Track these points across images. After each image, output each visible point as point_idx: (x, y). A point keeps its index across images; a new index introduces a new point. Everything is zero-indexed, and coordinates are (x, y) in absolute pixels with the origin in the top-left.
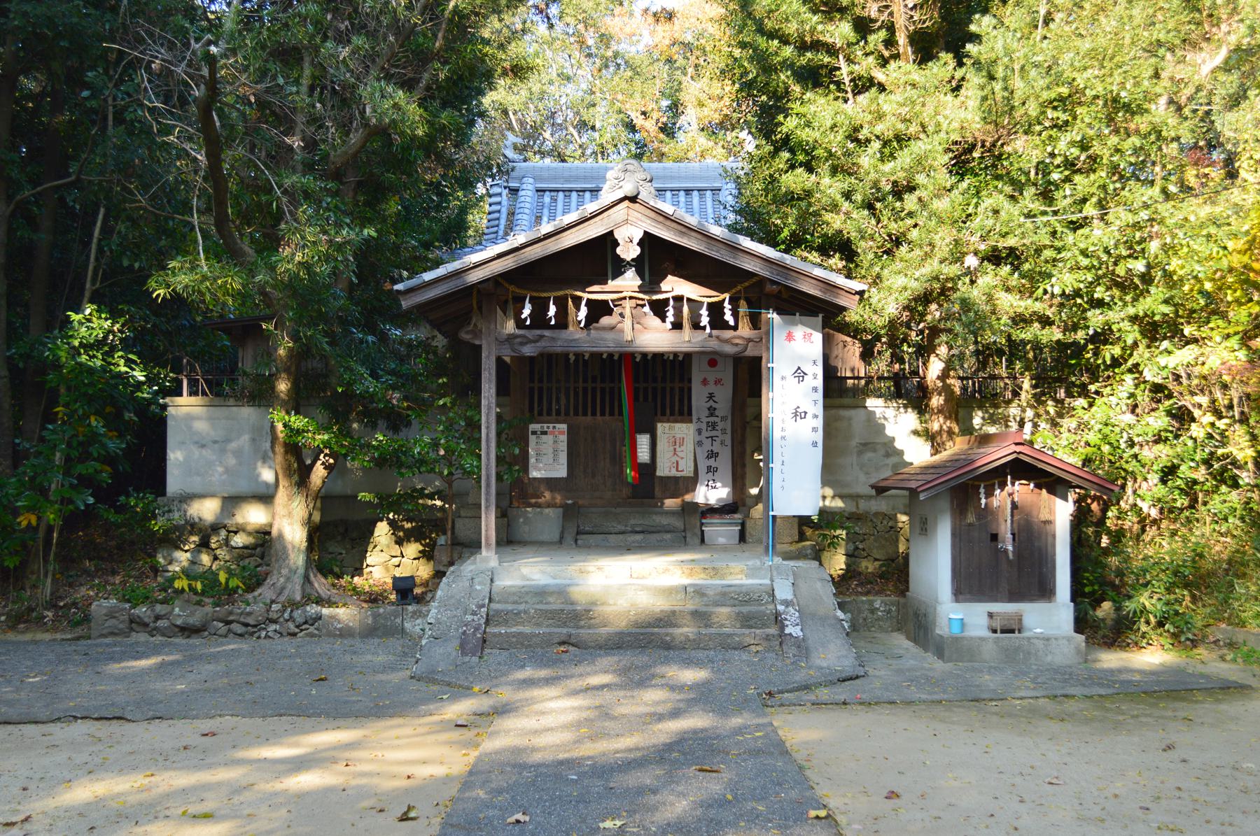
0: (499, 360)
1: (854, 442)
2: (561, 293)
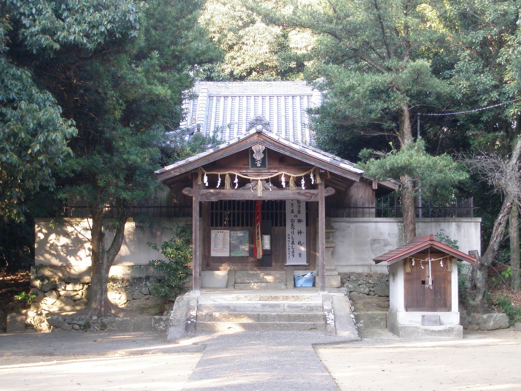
0: (200, 203)
1: (369, 239)
2: (289, 174)
